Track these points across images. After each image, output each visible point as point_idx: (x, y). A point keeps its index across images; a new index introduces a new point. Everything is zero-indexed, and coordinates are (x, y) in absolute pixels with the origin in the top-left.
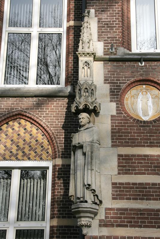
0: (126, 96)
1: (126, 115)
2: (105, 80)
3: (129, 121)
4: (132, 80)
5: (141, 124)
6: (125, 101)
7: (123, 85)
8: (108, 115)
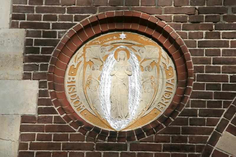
0: (72, 62)
1: (62, 116)
2: (14, 17)
3: (69, 133)
4: (90, 17)
5: (101, 142)
6: (67, 77)
7: (62, 30)
8: (14, 116)
